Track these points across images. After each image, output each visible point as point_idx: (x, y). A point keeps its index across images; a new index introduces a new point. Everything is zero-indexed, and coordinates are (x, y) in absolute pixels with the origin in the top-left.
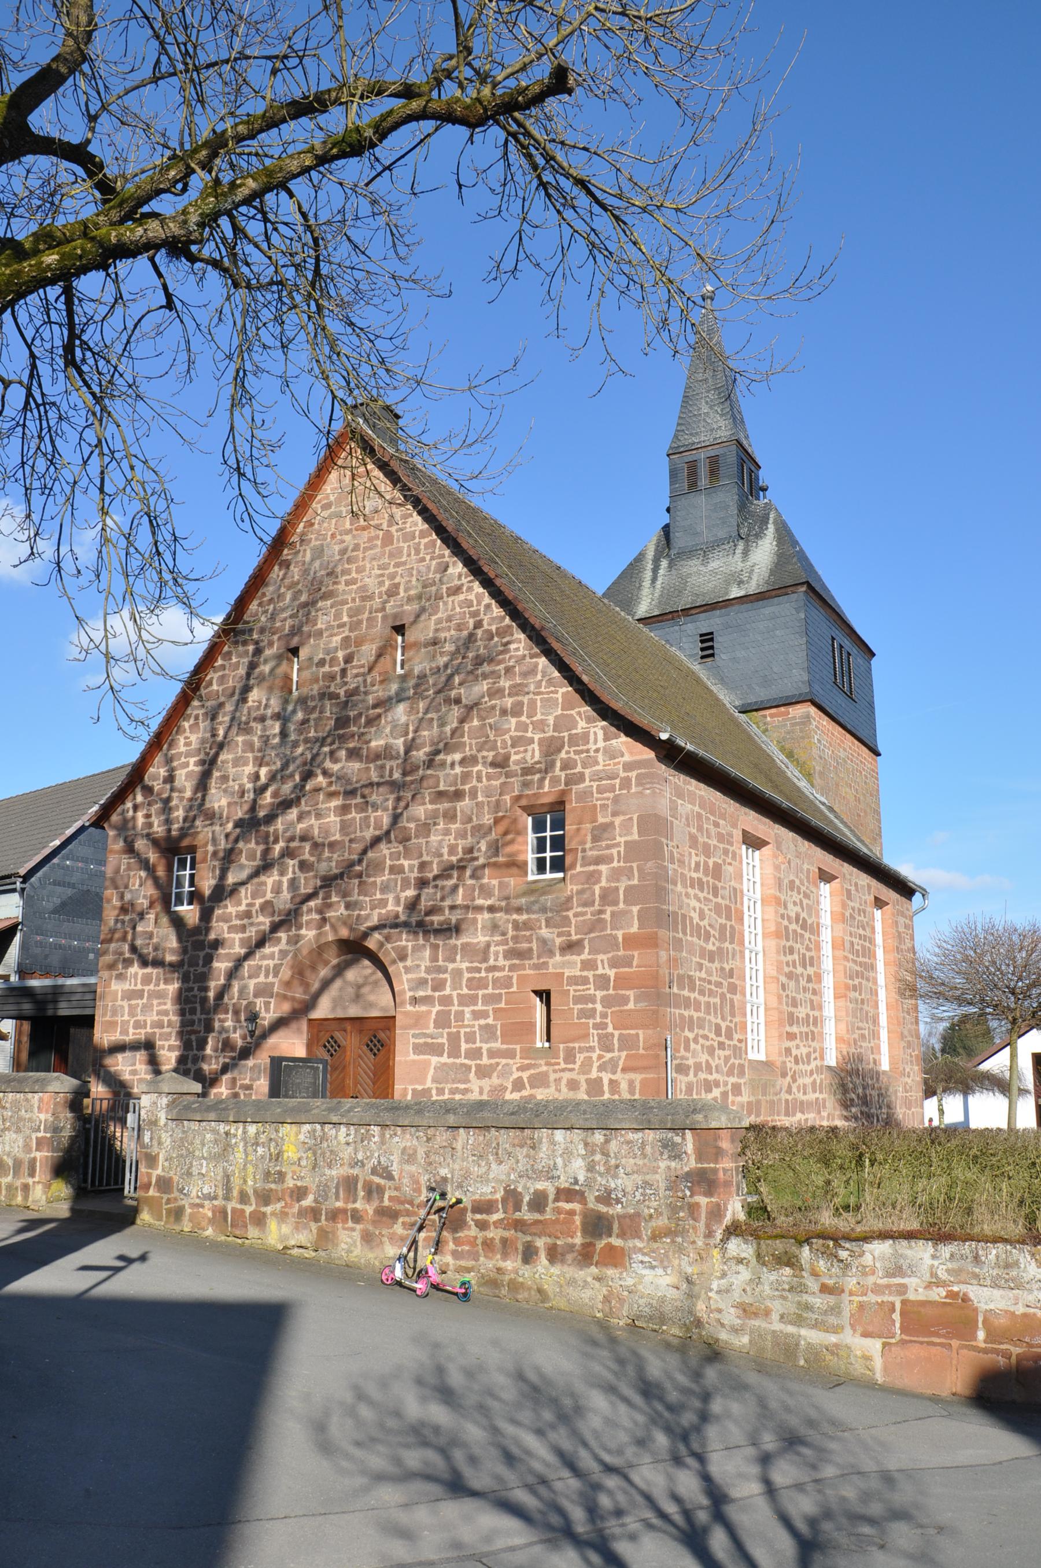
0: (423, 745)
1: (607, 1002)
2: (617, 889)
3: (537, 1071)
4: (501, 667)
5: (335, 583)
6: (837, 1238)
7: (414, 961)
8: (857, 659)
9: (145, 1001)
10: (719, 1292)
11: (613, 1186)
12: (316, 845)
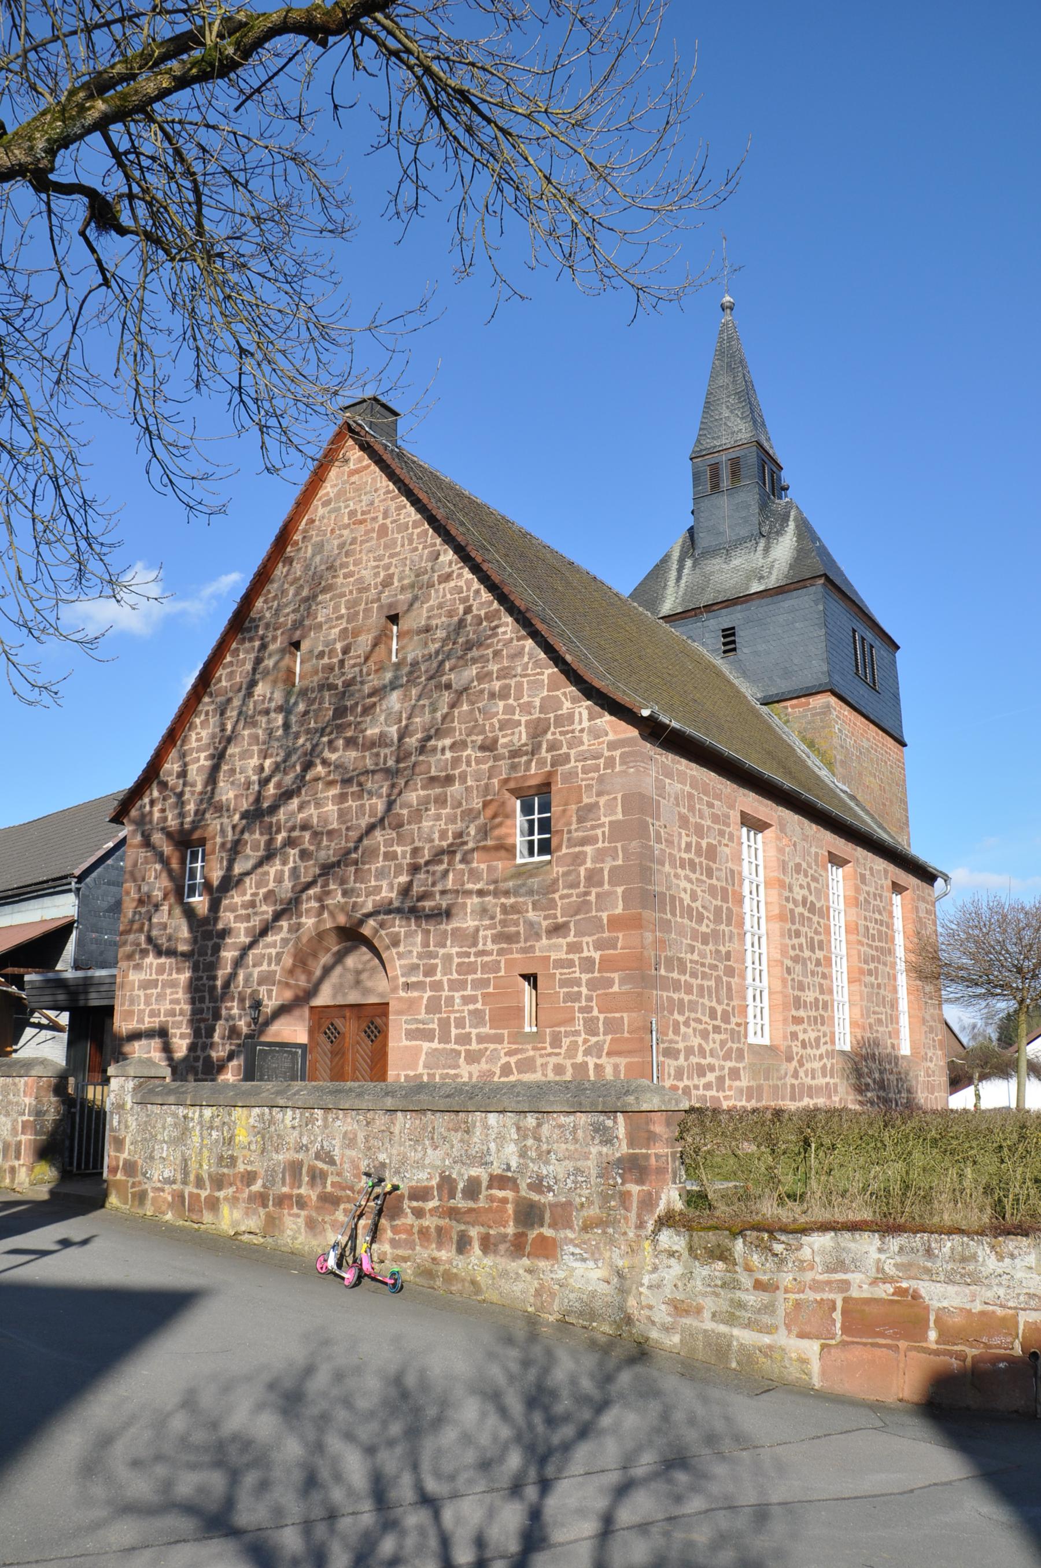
0: (416, 732)
1: (592, 985)
2: (602, 869)
3: (524, 1056)
4: (490, 651)
5: (334, 577)
6: (773, 1229)
7: (407, 946)
8: (880, 651)
9: (159, 990)
10: (650, 1287)
11: (545, 1172)
12: (316, 834)
